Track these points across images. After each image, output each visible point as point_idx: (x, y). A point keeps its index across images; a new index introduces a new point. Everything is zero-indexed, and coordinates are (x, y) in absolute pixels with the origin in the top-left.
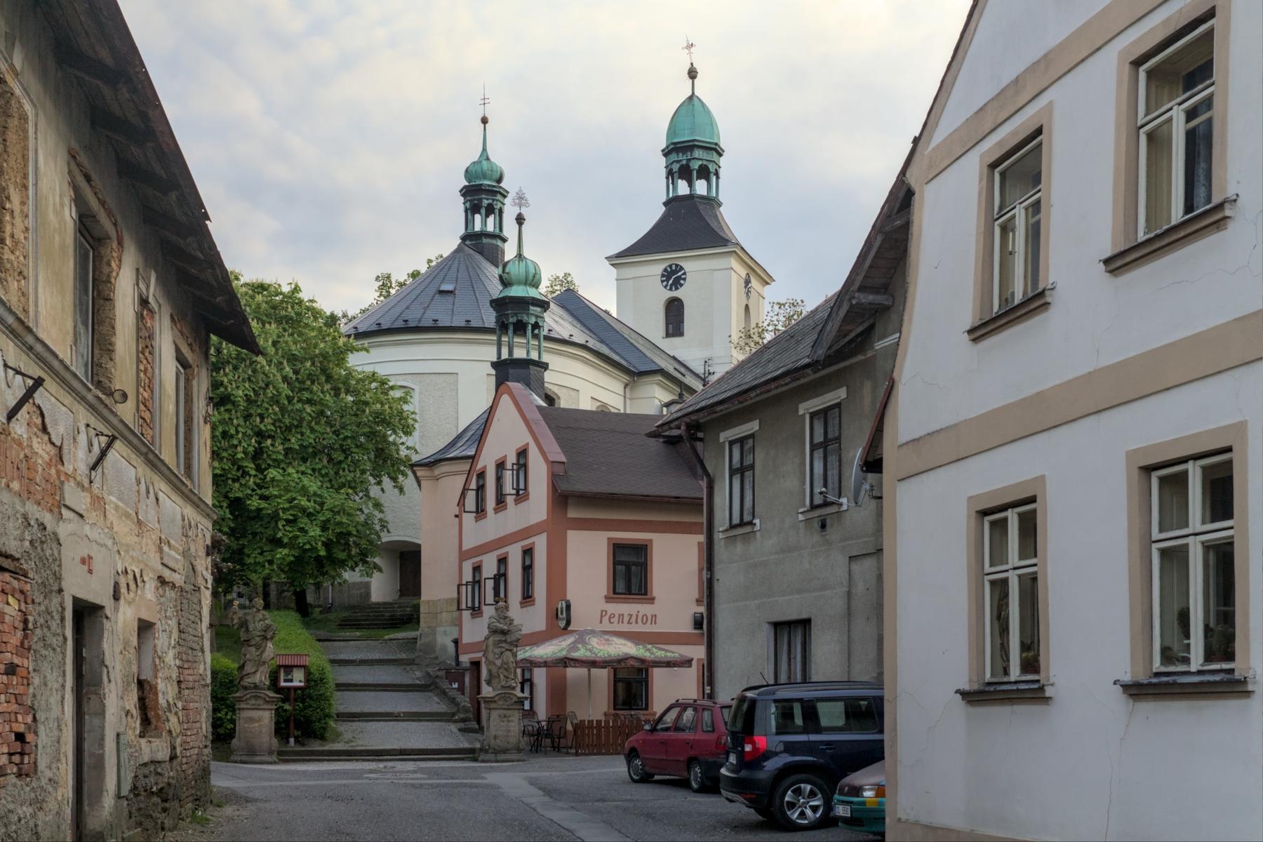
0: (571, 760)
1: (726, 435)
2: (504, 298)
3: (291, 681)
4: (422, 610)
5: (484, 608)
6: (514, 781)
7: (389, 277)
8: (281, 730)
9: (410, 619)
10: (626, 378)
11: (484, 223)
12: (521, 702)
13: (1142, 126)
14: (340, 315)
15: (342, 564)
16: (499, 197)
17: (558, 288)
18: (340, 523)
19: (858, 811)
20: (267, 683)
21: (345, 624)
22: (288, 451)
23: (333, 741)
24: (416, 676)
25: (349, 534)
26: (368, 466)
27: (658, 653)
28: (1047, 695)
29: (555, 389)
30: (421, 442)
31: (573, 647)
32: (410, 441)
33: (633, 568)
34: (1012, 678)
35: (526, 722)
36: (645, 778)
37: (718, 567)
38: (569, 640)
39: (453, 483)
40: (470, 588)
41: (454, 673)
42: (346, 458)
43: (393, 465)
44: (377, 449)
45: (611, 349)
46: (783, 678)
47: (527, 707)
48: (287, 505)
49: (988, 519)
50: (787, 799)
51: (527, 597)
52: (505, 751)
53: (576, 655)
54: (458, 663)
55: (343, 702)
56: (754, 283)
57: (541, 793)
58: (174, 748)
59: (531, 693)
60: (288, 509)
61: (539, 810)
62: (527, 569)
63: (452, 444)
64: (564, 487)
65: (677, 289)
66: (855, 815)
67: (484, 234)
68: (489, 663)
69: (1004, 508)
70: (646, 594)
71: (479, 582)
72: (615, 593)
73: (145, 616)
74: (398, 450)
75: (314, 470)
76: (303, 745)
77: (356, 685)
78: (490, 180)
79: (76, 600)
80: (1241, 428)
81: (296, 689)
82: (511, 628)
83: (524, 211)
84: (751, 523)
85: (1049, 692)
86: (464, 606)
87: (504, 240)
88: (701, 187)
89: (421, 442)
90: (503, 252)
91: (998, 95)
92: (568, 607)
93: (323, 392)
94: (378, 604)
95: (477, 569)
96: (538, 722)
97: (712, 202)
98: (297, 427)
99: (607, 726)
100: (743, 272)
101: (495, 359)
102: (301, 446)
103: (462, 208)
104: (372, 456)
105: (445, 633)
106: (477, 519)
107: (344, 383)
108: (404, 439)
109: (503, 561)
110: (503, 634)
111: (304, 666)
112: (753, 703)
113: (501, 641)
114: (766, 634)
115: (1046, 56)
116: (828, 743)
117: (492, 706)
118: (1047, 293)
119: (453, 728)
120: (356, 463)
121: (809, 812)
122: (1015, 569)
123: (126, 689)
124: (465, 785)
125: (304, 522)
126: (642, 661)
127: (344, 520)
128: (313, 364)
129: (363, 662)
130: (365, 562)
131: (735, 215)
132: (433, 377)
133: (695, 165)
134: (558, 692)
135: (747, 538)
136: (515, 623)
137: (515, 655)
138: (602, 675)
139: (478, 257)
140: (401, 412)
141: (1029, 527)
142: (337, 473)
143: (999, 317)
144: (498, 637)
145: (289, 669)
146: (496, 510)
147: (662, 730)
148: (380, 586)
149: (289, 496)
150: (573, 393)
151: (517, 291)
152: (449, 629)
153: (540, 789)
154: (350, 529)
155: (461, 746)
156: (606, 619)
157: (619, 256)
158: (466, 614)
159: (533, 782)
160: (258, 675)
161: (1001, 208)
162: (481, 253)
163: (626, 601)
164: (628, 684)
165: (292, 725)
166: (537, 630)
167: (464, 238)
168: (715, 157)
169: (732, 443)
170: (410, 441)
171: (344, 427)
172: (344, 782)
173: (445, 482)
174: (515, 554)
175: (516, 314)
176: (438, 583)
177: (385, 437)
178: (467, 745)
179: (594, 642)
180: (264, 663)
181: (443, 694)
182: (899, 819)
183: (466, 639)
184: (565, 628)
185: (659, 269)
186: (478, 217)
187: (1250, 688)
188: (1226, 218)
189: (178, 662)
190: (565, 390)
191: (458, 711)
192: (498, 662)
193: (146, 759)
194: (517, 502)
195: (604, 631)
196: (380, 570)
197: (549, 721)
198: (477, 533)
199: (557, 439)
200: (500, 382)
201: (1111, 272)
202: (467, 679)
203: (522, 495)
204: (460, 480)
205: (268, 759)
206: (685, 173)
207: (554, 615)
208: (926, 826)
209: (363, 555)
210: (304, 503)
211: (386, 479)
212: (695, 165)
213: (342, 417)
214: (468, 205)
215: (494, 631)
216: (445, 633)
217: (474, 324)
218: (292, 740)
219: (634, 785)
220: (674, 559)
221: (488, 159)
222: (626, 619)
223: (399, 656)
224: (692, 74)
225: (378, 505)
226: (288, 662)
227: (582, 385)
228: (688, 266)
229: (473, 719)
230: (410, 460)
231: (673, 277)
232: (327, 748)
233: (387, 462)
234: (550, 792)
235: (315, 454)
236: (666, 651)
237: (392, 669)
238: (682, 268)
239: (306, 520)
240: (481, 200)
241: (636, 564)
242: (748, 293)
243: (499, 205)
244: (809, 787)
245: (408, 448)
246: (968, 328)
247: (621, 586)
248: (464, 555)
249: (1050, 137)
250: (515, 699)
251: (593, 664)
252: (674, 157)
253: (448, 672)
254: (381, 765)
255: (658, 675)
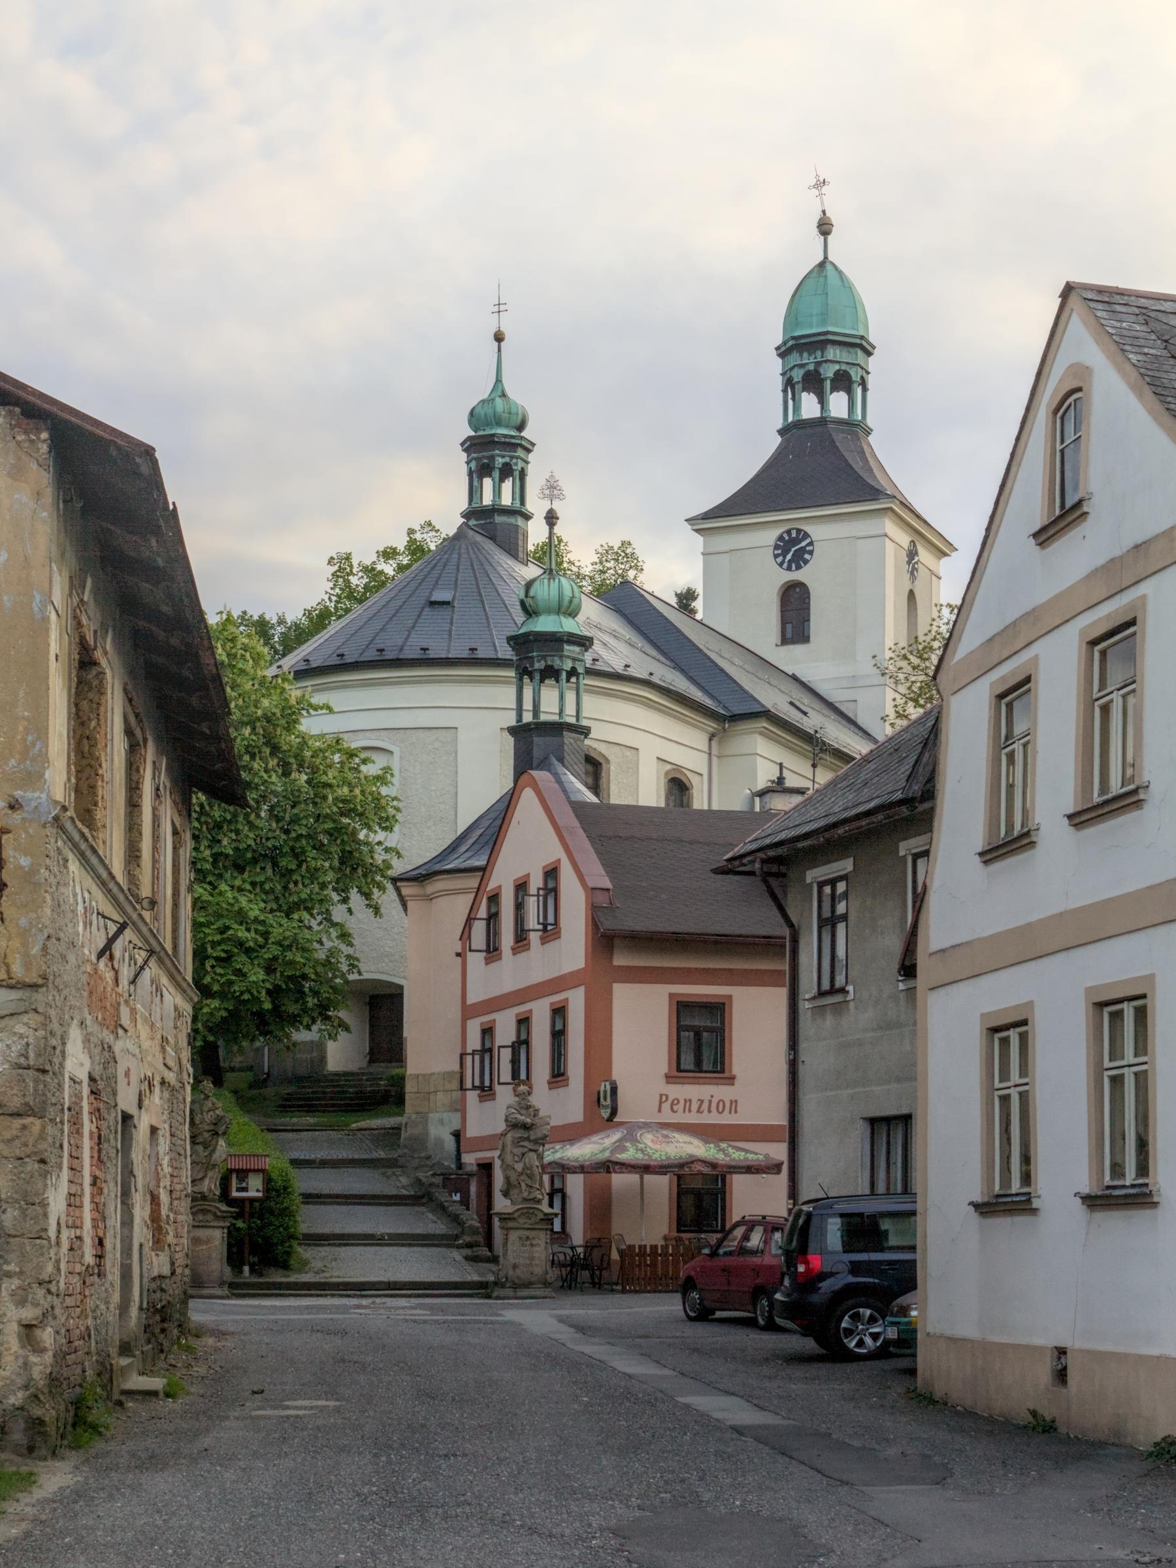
0: (617, 1298)
1: (814, 875)
2: (527, 634)
3: (245, 1189)
4: (409, 1087)
5: (498, 1089)
6: (539, 1319)
7: (348, 558)
8: (235, 1258)
9: (391, 1097)
10: (712, 725)
11: (497, 492)
12: (548, 1219)
13: (1097, 700)
14: (274, 621)
15: (294, 1020)
16: (520, 453)
17: (611, 564)
18: (291, 963)
19: (904, 1331)
20: (218, 1193)
21: (288, 1105)
22: (216, 857)
23: (300, 1271)
24: (400, 1184)
25: (304, 977)
26: (330, 876)
27: (734, 1154)
28: (1034, 1206)
29: (602, 748)
30: (411, 842)
31: (619, 1147)
32: (392, 839)
33: (705, 1034)
34: (1014, 1191)
35: (557, 1248)
36: (703, 1315)
37: (803, 1045)
38: (616, 1136)
39: (453, 905)
40: (477, 1058)
41: (455, 1179)
42: (299, 866)
43: (365, 875)
44: (343, 851)
45: (691, 679)
46: (881, 1188)
47: (557, 1227)
48: (218, 937)
49: (998, 1036)
50: (844, 1325)
51: (558, 1075)
52: (528, 1285)
53: (622, 1157)
54: (460, 1166)
55: (311, 1219)
56: (925, 556)
57: (573, 1330)
58: (172, 1264)
59: (563, 1209)
60: (219, 943)
61: (569, 1345)
62: (558, 1036)
63: (452, 848)
64: (608, 924)
65: (798, 567)
66: (903, 1336)
67: (496, 510)
68: (506, 1167)
69: (1007, 1027)
70: (723, 1071)
71: (490, 1050)
72: (679, 1070)
73: (154, 1123)
74: (371, 851)
75: (253, 884)
76: (261, 1275)
77: (319, 1196)
78: (507, 426)
79: (122, 1111)
80: (1151, 978)
81: (252, 1200)
82: (537, 1121)
83: (557, 506)
84: (843, 990)
85: (1036, 1203)
86: (469, 1085)
87: (527, 517)
88: (838, 404)
89: (411, 842)
90: (525, 536)
91: (1003, 631)
92: (614, 1090)
93: (266, 771)
94: (337, 1074)
95: (488, 1032)
96: (573, 1248)
97: (855, 428)
98: (230, 822)
99: (665, 1254)
100: (904, 539)
101: (513, 723)
102: (236, 849)
103: (464, 469)
104: (336, 863)
105: (441, 1122)
106: (488, 961)
107: (296, 757)
108: (381, 836)
109: (524, 1022)
110: (525, 1129)
111: (263, 1171)
112: (809, 1215)
113: (522, 1139)
114: (859, 1134)
115: (1034, 610)
116: (891, 1263)
117: (511, 1224)
118: (1032, 833)
119: (457, 1255)
120: (314, 874)
121: (868, 1340)
122: (1016, 1086)
123: (145, 1195)
124: (479, 1322)
125: (240, 961)
126: (714, 1165)
127: (298, 959)
128: (254, 729)
129: (324, 1164)
130: (327, 1018)
131: (892, 452)
132: (421, 733)
133: (829, 371)
134: (601, 1208)
135: (839, 1009)
136: (541, 1114)
137: (540, 1157)
138: (661, 1185)
139: (489, 546)
140: (377, 798)
141: (1141, 1015)
142: (285, 888)
143: (1005, 845)
144: (520, 1133)
145: (243, 1174)
146: (515, 951)
147: (726, 1254)
148: (342, 1053)
149: (219, 924)
150: (628, 753)
151: (545, 624)
152: (446, 1116)
153: (571, 1326)
154: (307, 970)
155: (469, 1278)
156: (666, 1106)
157: (706, 516)
158: (472, 1097)
159: (561, 1320)
160: (207, 1181)
161: (1007, 739)
162: (492, 538)
163: (695, 1081)
164: (698, 1195)
165: (247, 1251)
166: (571, 1121)
167: (467, 515)
168: (860, 356)
169: (821, 885)
170: (392, 839)
171: (295, 820)
172: (330, 1316)
173: (442, 902)
174: (540, 1011)
175: (544, 657)
176: (431, 1046)
177: (354, 833)
178: (476, 1278)
179: (648, 1138)
180: (214, 1166)
181: (442, 1208)
182: (928, 1334)
183: (472, 1131)
184: (610, 1119)
185: (770, 536)
186: (488, 483)
187: (1155, 1199)
188: (1140, 800)
189: (170, 1169)
190: (616, 749)
191: (463, 1233)
192: (519, 1167)
193: (156, 1274)
194: (544, 940)
195: (661, 1124)
196: (347, 1029)
197: (589, 1247)
198: (487, 980)
199: (598, 853)
200: (524, 764)
201: (1075, 825)
202: (473, 1189)
203: (551, 931)
204: (462, 904)
205: (219, 1292)
206: (813, 382)
207: (594, 1100)
208: (950, 1338)
209: (323, 1008)
210: (242, 934)
211: (355, 896)
212: (829, 371)
213: (293, 807)
214: (473, 465)
215: (514, 1125)
216: (441, 1122)
217: (481, 654)
218: (246, 1269)
219: (688, 1323)
220: (757, 1019)
221: (504, 395)
222: (695, 1107)
223: (375, 1155)
224: (825, 228)
225: (345, 936)
226: (242, 1164)
227: (644, 747)
228: (816, 532)
229: (481, 1243)
230: (389, 867)
231: (793, 549)
232: (292, 1279)
233: (355, 869)
234: (582, 1329)
235: (255, 861)
236: (747, 1151)
237: (367, 1173)
238: (806, 535)
239: (243, 958)
240: (492, 458)
241: (707, 1029)
242: (913, 573)
243: (520, 464)
244: (868, 1312)
245: (387, 850)
246: (980, 850)
247: (688, 1060)
248: (468, 1012)
249: (1036, 683)
250: (541, 1216)
251: (646, 1169)
252: (794, 359)
253: (446, 1178)
254: (364, 1302)
255: (738, 1182)
